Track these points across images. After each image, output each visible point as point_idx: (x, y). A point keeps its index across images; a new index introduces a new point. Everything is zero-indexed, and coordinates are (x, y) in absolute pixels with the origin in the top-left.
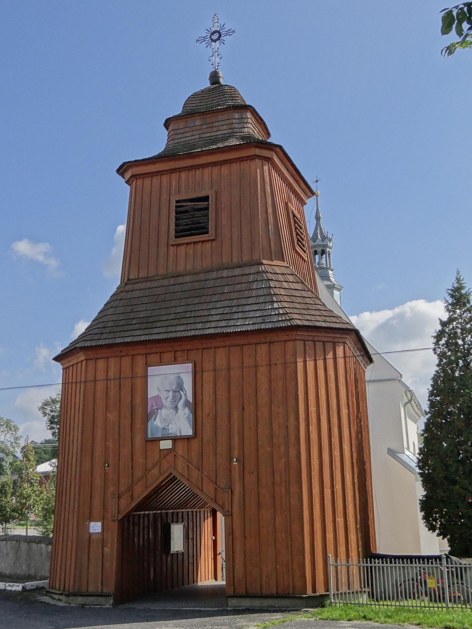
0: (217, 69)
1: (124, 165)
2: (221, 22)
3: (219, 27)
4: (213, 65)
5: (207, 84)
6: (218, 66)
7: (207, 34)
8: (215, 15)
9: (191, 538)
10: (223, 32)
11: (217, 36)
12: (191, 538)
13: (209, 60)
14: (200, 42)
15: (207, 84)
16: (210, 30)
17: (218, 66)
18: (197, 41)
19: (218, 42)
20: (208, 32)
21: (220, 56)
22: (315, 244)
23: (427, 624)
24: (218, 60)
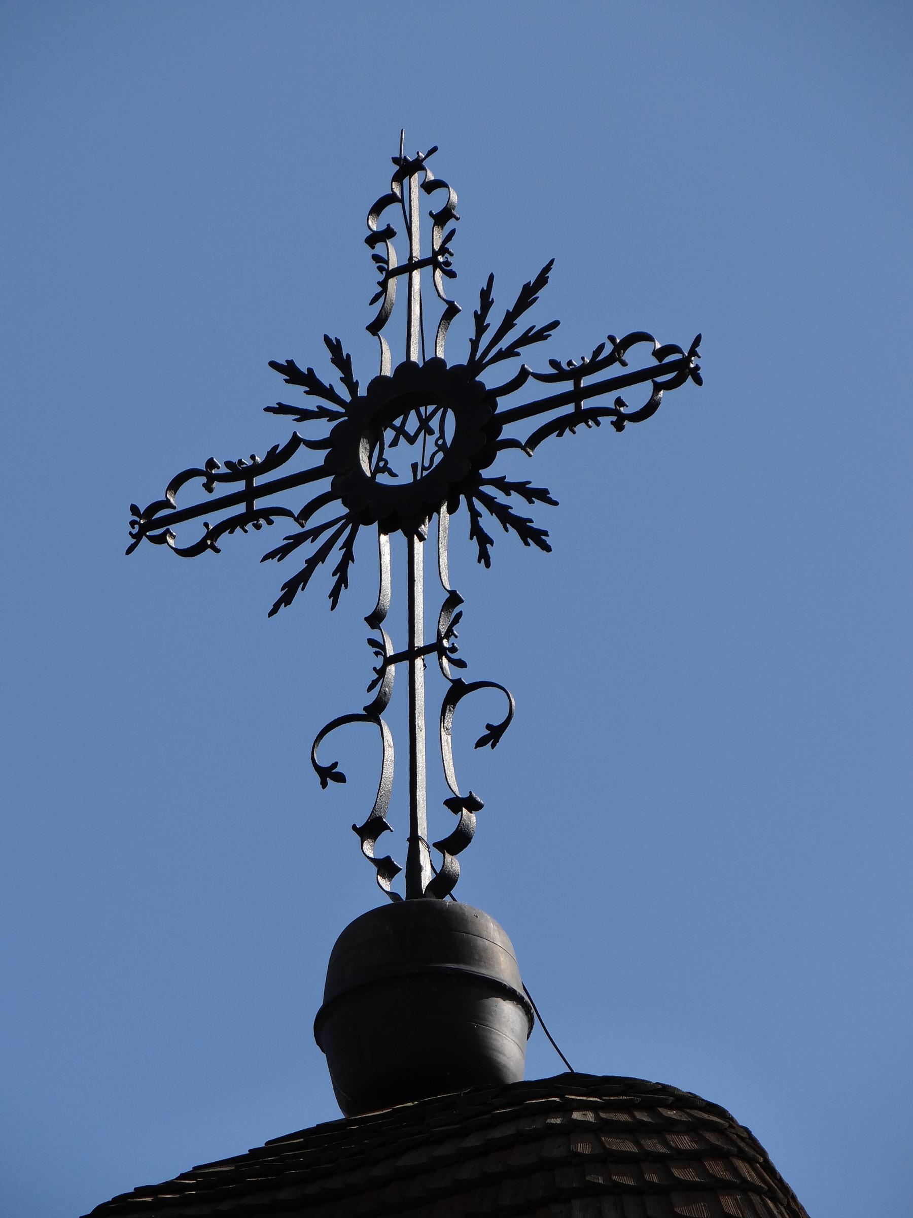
0: (444, 881)
1: (714, 1114)
2: (492, 256)
3: (464, 324)
4: (373, 828)
5: (295, 1094)
6: (457, 842)
7: (282, 430)
8: (406, 168)
9: (674, 1142)
10: (517, 379)
11: (419, 439)
12: (674, 1142)
13: (329, 774)
14: (188, 532)
15: (295, 1094)
16: (330, 375)
17: (457, 842)
18: (151, 523)
19: (447, 525)
20: (298, 396)
21: (480, 709)
22: (302, 530)
23: (449, 633)
24: (447, 758)
